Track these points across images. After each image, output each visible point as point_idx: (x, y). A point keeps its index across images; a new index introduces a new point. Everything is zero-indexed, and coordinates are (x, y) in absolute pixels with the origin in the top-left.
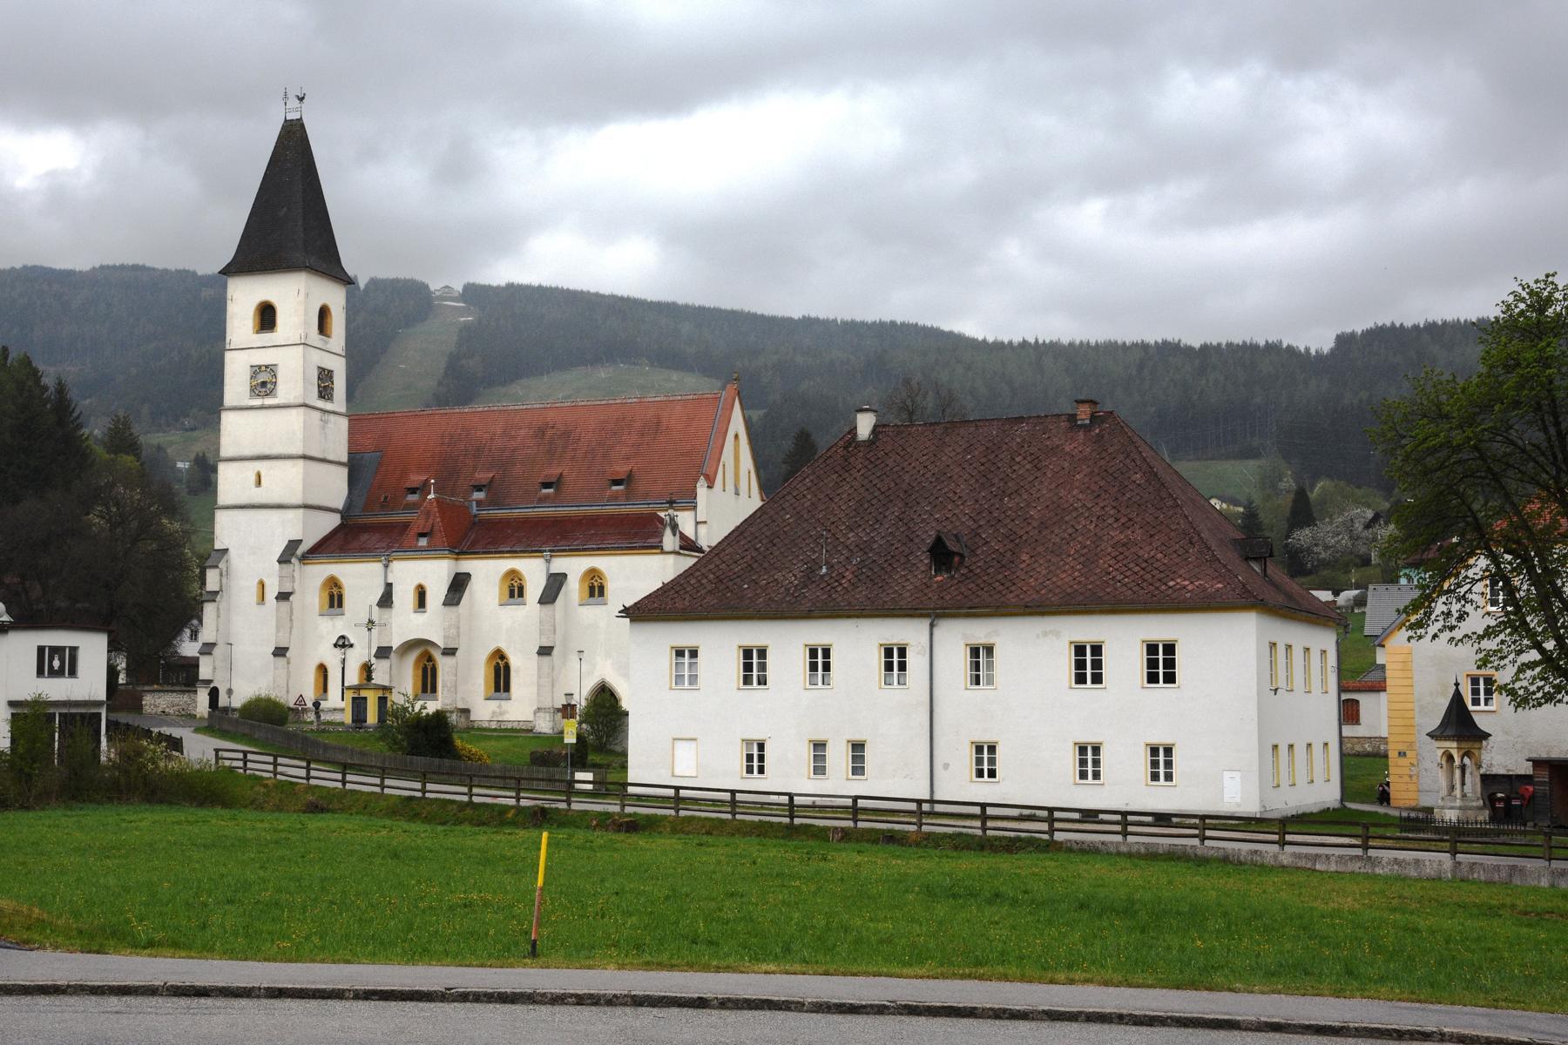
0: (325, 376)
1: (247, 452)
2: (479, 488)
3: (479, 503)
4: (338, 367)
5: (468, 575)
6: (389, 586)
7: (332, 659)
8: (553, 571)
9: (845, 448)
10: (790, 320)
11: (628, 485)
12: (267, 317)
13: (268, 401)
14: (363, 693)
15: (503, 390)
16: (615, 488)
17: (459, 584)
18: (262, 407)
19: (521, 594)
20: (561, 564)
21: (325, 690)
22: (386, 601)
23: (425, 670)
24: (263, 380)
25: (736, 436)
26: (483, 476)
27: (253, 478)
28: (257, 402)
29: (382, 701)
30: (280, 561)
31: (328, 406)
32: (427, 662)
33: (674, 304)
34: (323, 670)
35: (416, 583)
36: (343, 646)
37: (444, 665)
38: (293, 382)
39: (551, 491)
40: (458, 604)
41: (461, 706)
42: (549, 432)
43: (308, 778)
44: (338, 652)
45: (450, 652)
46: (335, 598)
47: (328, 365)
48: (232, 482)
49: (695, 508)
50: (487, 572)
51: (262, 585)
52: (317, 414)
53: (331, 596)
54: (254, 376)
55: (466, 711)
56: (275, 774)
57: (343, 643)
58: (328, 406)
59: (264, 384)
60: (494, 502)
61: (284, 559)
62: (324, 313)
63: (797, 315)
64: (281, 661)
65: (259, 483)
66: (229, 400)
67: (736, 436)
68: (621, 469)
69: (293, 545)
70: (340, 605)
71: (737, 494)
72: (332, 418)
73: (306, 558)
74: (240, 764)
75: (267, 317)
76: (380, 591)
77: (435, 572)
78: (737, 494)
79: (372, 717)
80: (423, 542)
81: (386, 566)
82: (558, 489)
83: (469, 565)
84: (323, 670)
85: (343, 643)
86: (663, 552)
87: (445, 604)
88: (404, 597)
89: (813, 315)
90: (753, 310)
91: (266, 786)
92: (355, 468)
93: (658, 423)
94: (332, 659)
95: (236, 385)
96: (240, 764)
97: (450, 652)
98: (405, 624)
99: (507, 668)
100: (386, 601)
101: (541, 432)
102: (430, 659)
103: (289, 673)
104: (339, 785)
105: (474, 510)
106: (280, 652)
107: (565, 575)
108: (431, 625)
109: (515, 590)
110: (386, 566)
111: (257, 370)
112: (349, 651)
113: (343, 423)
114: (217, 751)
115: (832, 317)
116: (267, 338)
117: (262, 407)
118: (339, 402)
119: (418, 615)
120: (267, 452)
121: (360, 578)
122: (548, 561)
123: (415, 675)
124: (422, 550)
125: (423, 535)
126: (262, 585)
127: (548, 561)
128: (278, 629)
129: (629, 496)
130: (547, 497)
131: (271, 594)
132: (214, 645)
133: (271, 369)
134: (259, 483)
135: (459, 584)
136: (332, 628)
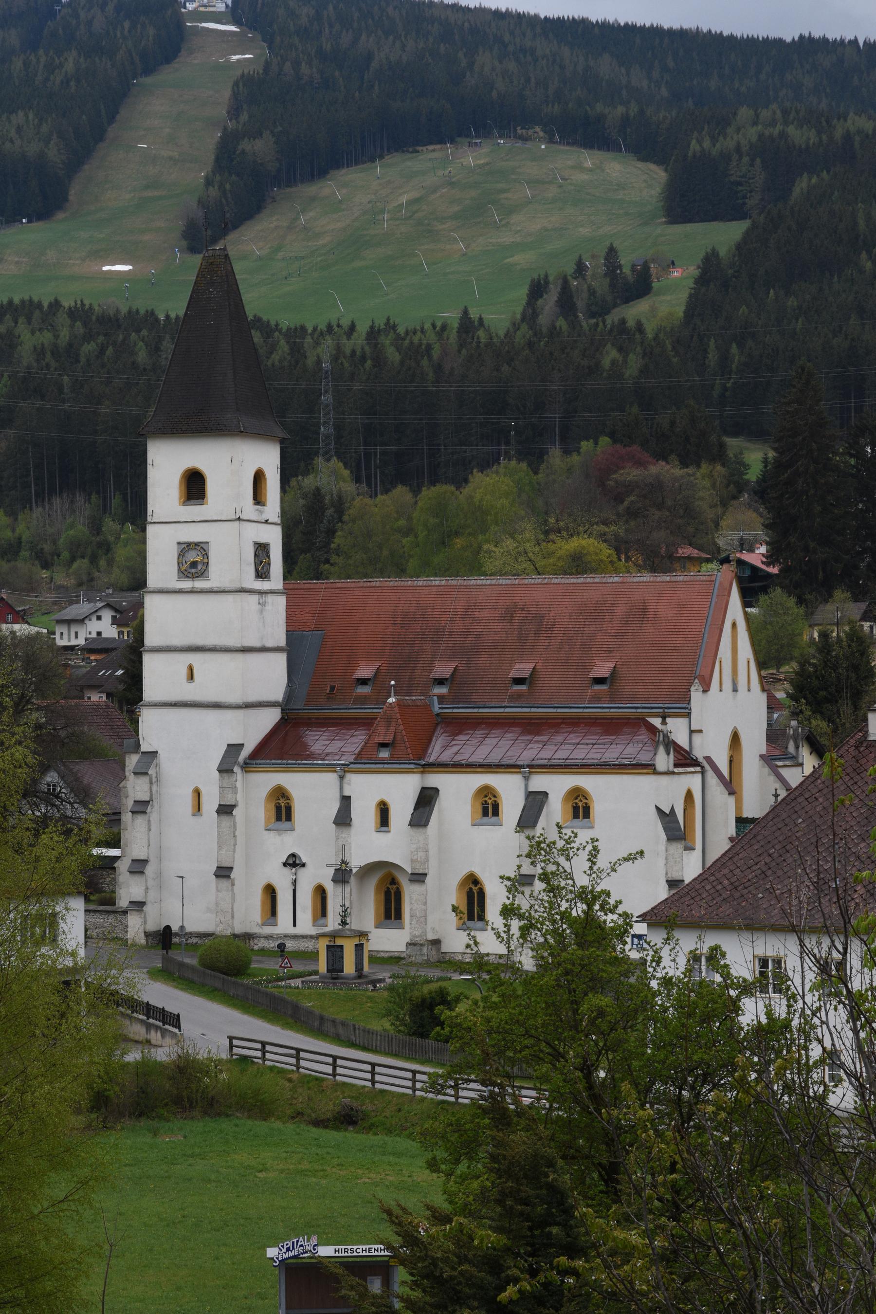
0: (262, 549)
1: (177, 642)
2: (440, 682)
3: (441, 698)
4: (274, 537)
5: (436, 790)
6: (346, 801)
7: (282, 880)
8: (532, 789)
9: (857, 747)
10: (779, 42)
11: (612, 685)
12: (194, 486)
13: (199, 584)
14: (339, 942)
15: (311, 189)
16: (597, 687)
17: (426, 800)
18: (192, 592)
19: (496, 813)
20: (539, 782)
21: (274, 913)
22: (343, 819)
23: (387, 893)
24: (193, 561)
25: (734, 625)
26: (443, 669)
27: (184, 672)
28: (187, 584)
29: (359, 948)
30: (220, 771)
31: (264, 585)
32: (390, 890)
33: (584, 22)
34: (270, 892)
35: (377, 799)
36: (294, 865)
37: (411, 894)
38: (230, 563)
39: (524, 688)
40: (425, 824)
41: (431, 936)
42: (519, 615)
43: (334, 1074)
44: (288, 873)
45: (419, 878)
46: (282, 809)
47: (263, 539)
48: (159, 676)
49: (688, 715)
50: (457, 791)
51: (197, 793)
52: (254, 598)
53: (278, 808)
54: (181, 554)
55: (436, 943)
56: (298, 1068)
57: (293, 862)
58: (264, 585)
59: (194, 564)
60: (455, 698)
61: (225, 769)
62: (259, 478)
63: (789, 35)
64: (224, 883)
65: (191, 677)
66: (153, 581)
67: (734, 625)
68: (603, 669)
69: (234, 749)
70: (289, 818)
71: (735, 690)
72: (270, 598)
73: (248, 766)
74: (259, 1054)
75: (194, 486)
76: (335, 806)
77: (400, 789)
78: (735, 690)
79: (349, 968)
80: (384, 754)
81: (342, 778)
82: (531, 685)
83: (435, 780)
84: (270, 892)
85: (293, 862)
86: (656, 773)
87: (411, 824)
88: (364, 813)
89: (817, 34)
90: (716, 29)
91: (290, 1080)
92: (294, 648)
93: (645, 610)
94: (282, 880)
95: (161, 566)
96: (259, 1054)
97: (419, 878)
98: (367, 845)
99: (482, 894)
100: (343, 819)
101: (509, 614)
102: (394, 881)
103: (233, 895)
104: (369, 1084)
105: (436, 708)
106: (223, 872)
107: (545, 794)
108: (394, 846)
109: (488, 806)
110: (342, 778)
111: (186, 548)
112: (301, 872)
113: (280, 602)
114: (231, 1038)
115: (849, 37)
116: (194, 511)
117: (192, 592)
118: (276, 579)
119: (381, 835)
120: (200, 642)
121: (312, 791)
122: (527, 779)
123: (377, 902)
124: (383, 762)
125: (384, 745)
126: (197, 793)
127: (527, 779)
128: (220, 847)
129: (613, 696)
130: (519, 696)
131: (210, 804)
132: (145, 862)
133: (201, 547)
134: (191, 677)
135: (426, 800)
136: (281, 844)
